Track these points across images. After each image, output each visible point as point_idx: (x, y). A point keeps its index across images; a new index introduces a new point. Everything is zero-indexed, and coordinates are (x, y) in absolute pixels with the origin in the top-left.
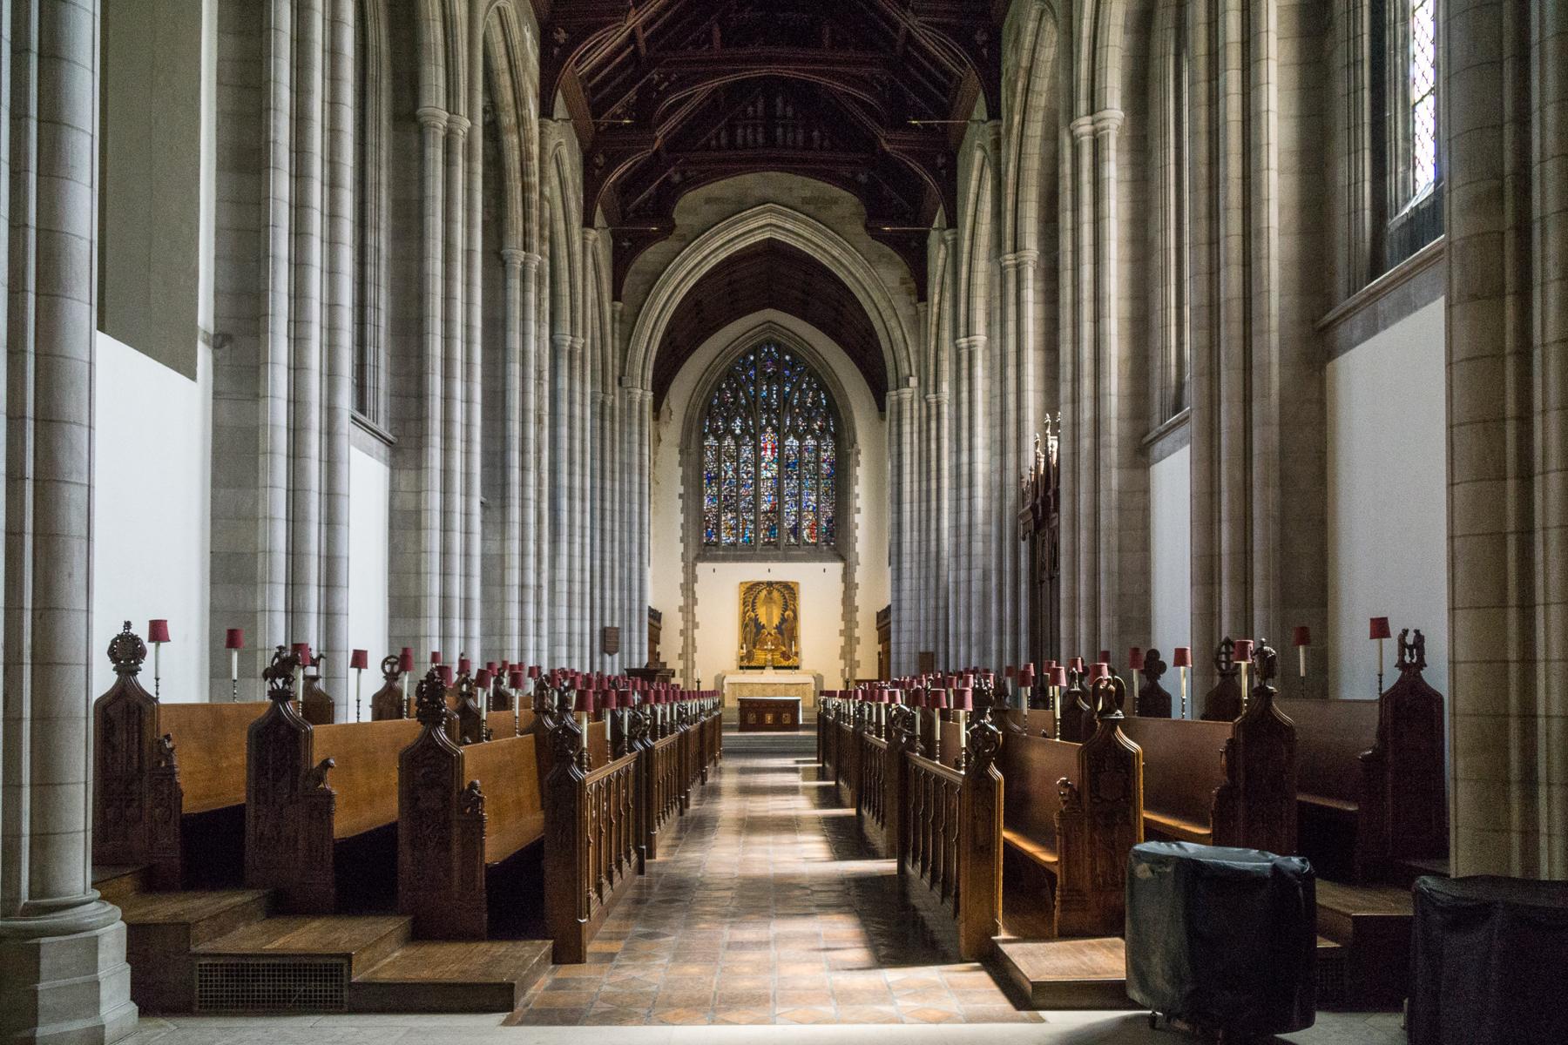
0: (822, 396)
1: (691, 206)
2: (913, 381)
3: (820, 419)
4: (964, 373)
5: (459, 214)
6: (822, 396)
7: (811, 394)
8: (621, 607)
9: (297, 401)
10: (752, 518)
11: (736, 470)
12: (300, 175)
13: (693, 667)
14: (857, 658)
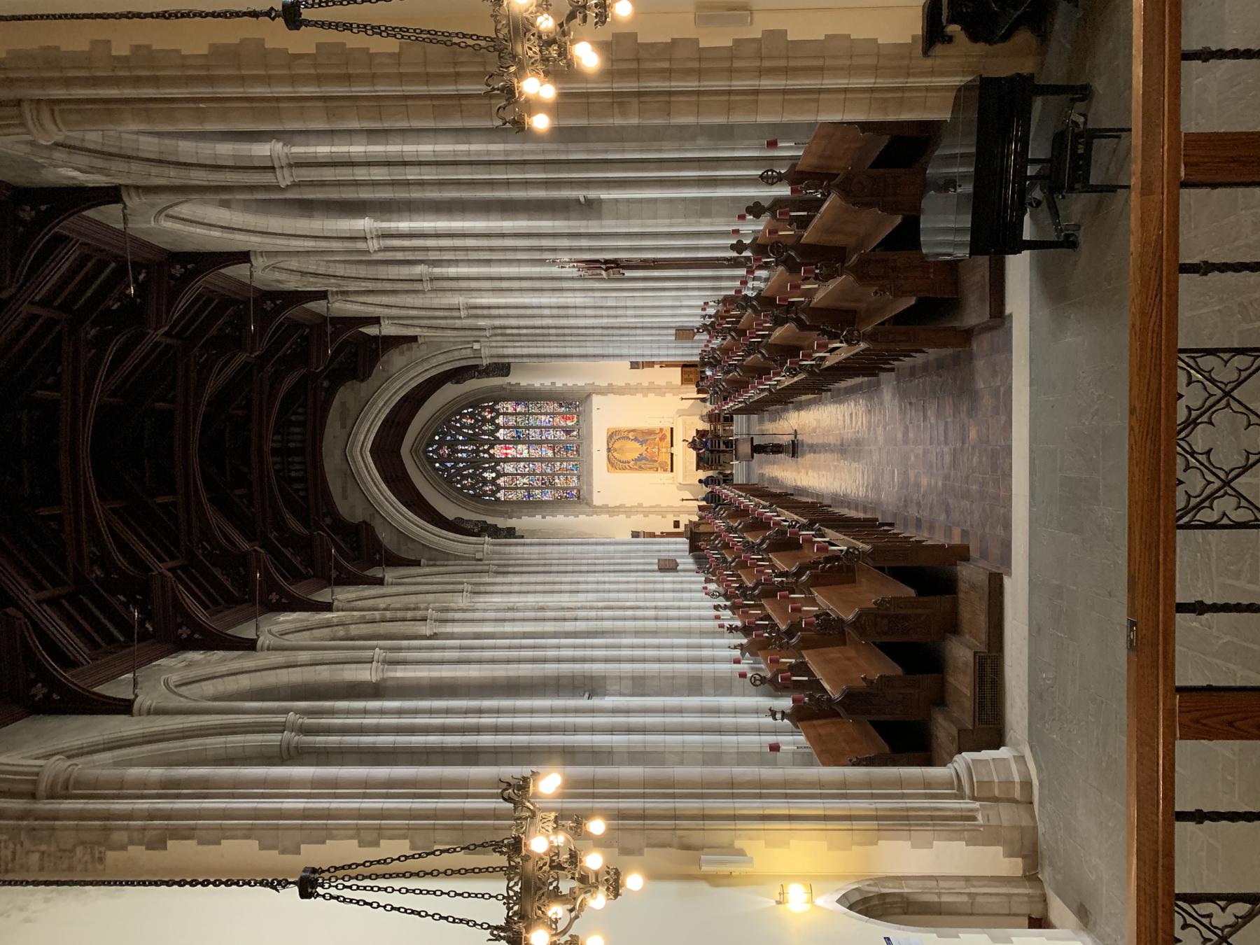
0: (465, 411)
1: (349, 509)
2: (476, 346)
3: (483, 413)
4: (486, 312)
5: (437, 655)
6: (465, 411)
7: (464, 420)
8: (643, 557)
9: (612, 730)
10: (558, 464)
11: (523, 475)
12: (478, 730)
13: (671, 507)
14: (664, 384)
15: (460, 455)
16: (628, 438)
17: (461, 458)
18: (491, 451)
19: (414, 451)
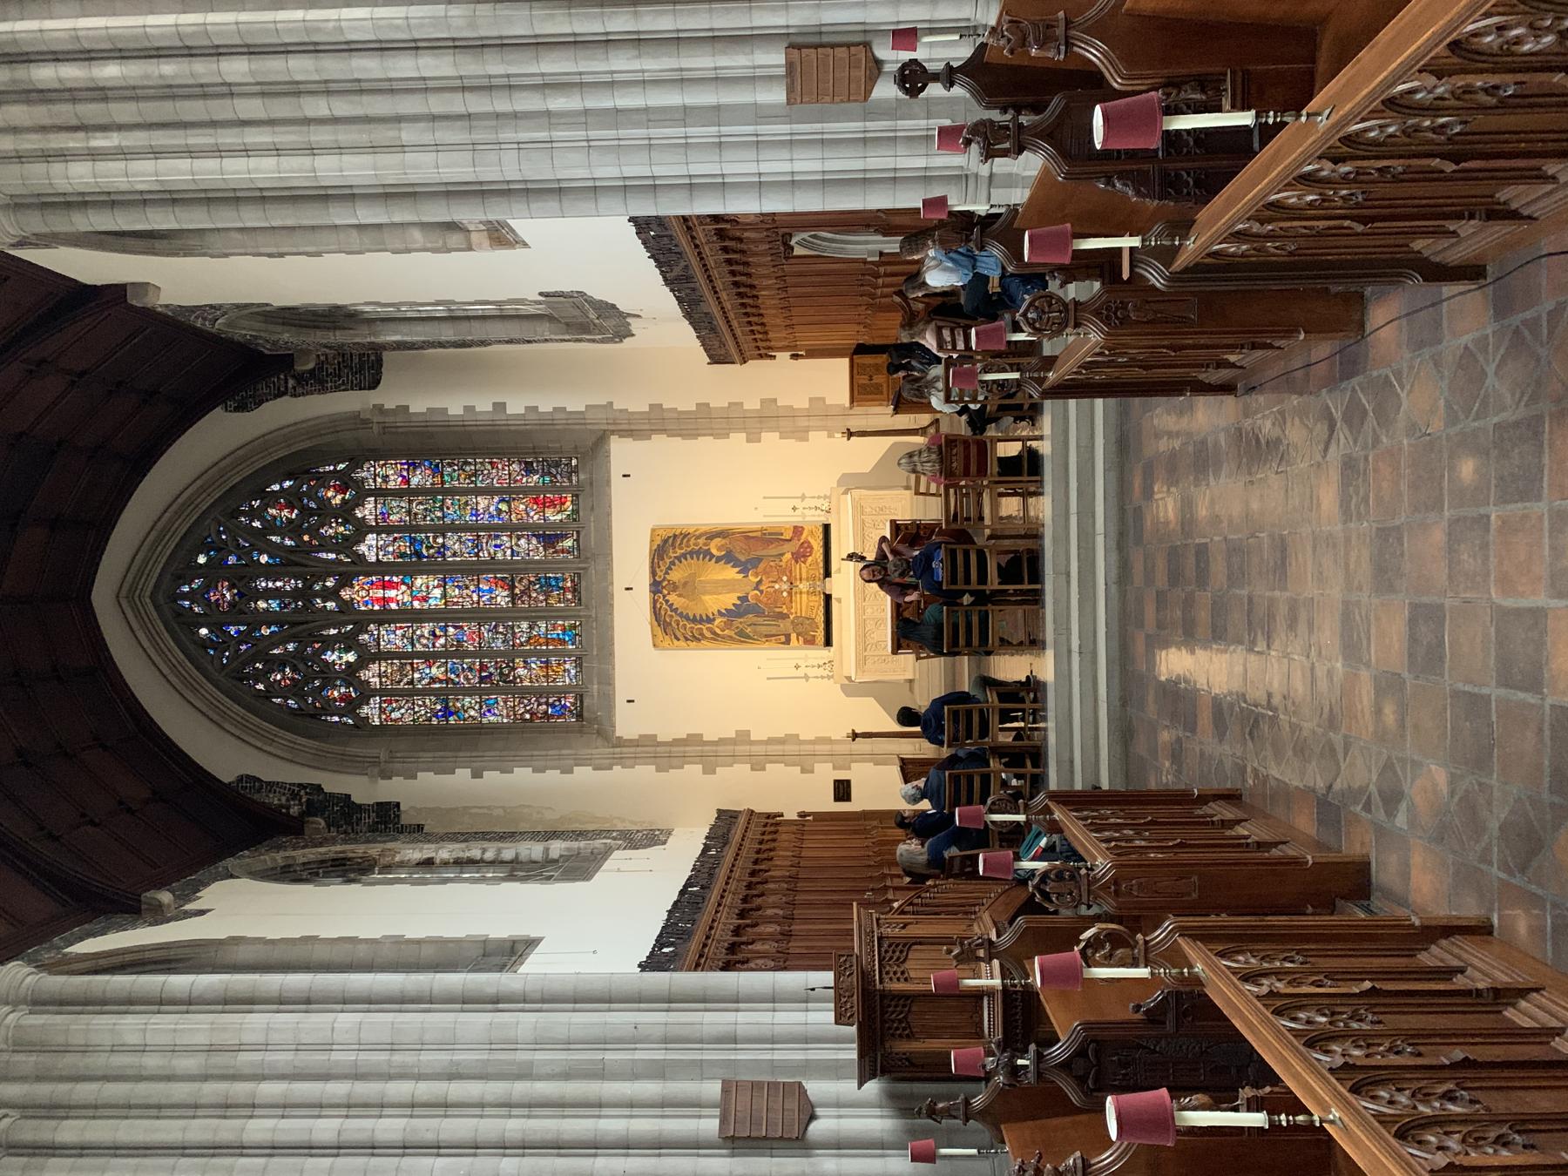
0: (276, 487)
6: (276, 487)
7: (273, 511)
8: (659, 1071)
10: (525, 625)
11: (430, 657)
15: (262, 604)
16: (708, 554)
17: (266, 611)
18: (345, 594)
19: (127, 595)
